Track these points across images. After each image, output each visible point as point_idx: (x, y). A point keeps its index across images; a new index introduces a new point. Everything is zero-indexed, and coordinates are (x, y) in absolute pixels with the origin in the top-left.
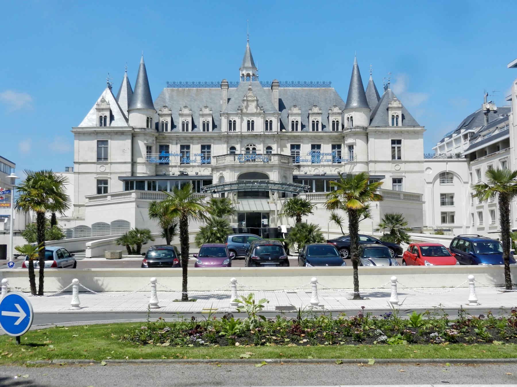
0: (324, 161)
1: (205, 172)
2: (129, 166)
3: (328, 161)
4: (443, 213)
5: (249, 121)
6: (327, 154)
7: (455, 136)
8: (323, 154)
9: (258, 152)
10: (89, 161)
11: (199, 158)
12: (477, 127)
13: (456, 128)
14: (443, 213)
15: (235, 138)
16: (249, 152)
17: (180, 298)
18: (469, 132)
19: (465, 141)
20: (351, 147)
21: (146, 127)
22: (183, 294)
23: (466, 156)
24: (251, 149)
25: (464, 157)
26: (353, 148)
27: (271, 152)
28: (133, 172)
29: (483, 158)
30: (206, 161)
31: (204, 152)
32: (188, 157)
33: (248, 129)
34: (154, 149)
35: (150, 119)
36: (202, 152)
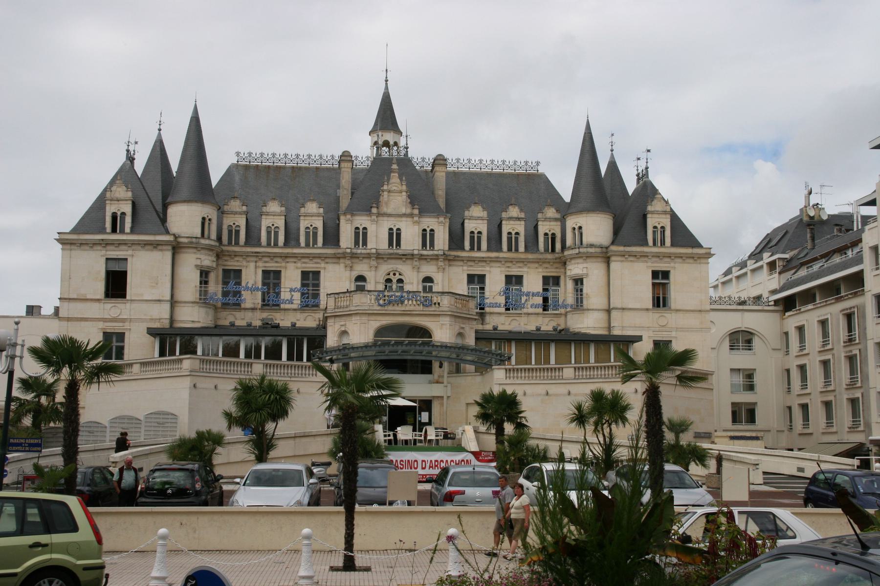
0: (529, 306)
1: (308, 321)
2: (167, 306)
3: (536, 306)
4: (734, 404)
5: (391, 229)
7: (751, 265)
8: (528, 294)
9: (407, 288)
10: (88, 297)
11: (297, 296)
14: (734, 404)
15: (365, 261)
16: (391, 287)
17: (340, 564)
18: (779, 259)
19: (771, 274)
20: (578, 282)
21: (199, 235)
22: (345, 556)
23: (776, 302)
24: (395, 281)
25: (772, 303)
26: (582, 284)
27: (431, 288)
28: (172, 320)
29: (810, 306)
30: (311, 301)
33: (390, 244)
34: (212, 277)
36: (303, 285)
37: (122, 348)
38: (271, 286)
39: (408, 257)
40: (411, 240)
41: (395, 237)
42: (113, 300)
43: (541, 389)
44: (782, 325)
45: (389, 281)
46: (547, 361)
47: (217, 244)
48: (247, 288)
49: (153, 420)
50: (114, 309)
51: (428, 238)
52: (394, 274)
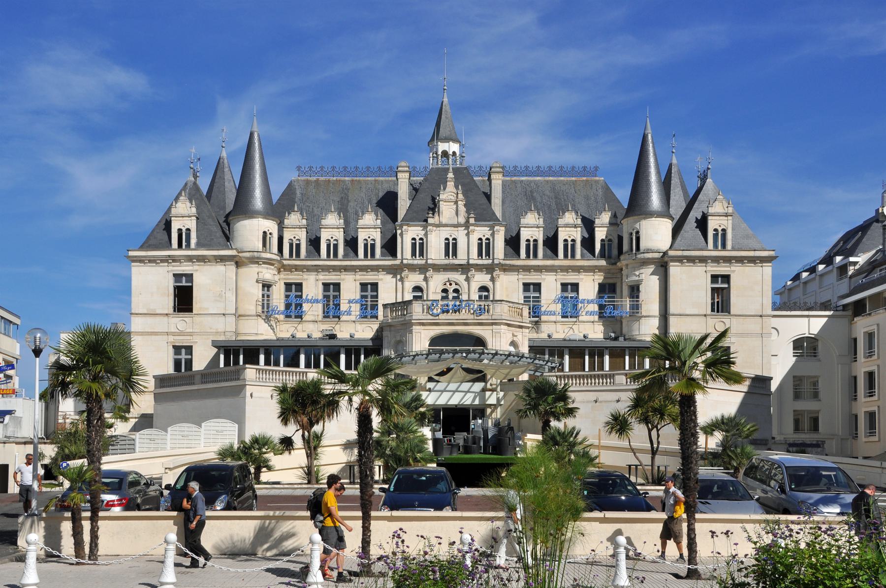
0: (584, 313)
3: (591, 313)
6: (589, 302)
8: (583, 301)
10: (158, 312)
11: (356, 308)
12: (864, 252)
13: (822, 253)
19: (841, 279)
24: (451, 291)
25: (841, 308)
31: (366, 297)
32: (338, 306)
35: (269, 236)
37: (191, 360)
38: (331, 298)
39: (465, 269)
40: (467, 251)
41: (451, 248)
42: (181, 314)
43: (592, 396)
44: (850, 330)
45: (445, 291)
46: (601, 368)
47: (279, 258)
48: (308, 301)
49: (212, 428)
50: (181, 322)
51: (485, 248)
52: (451, 284)
